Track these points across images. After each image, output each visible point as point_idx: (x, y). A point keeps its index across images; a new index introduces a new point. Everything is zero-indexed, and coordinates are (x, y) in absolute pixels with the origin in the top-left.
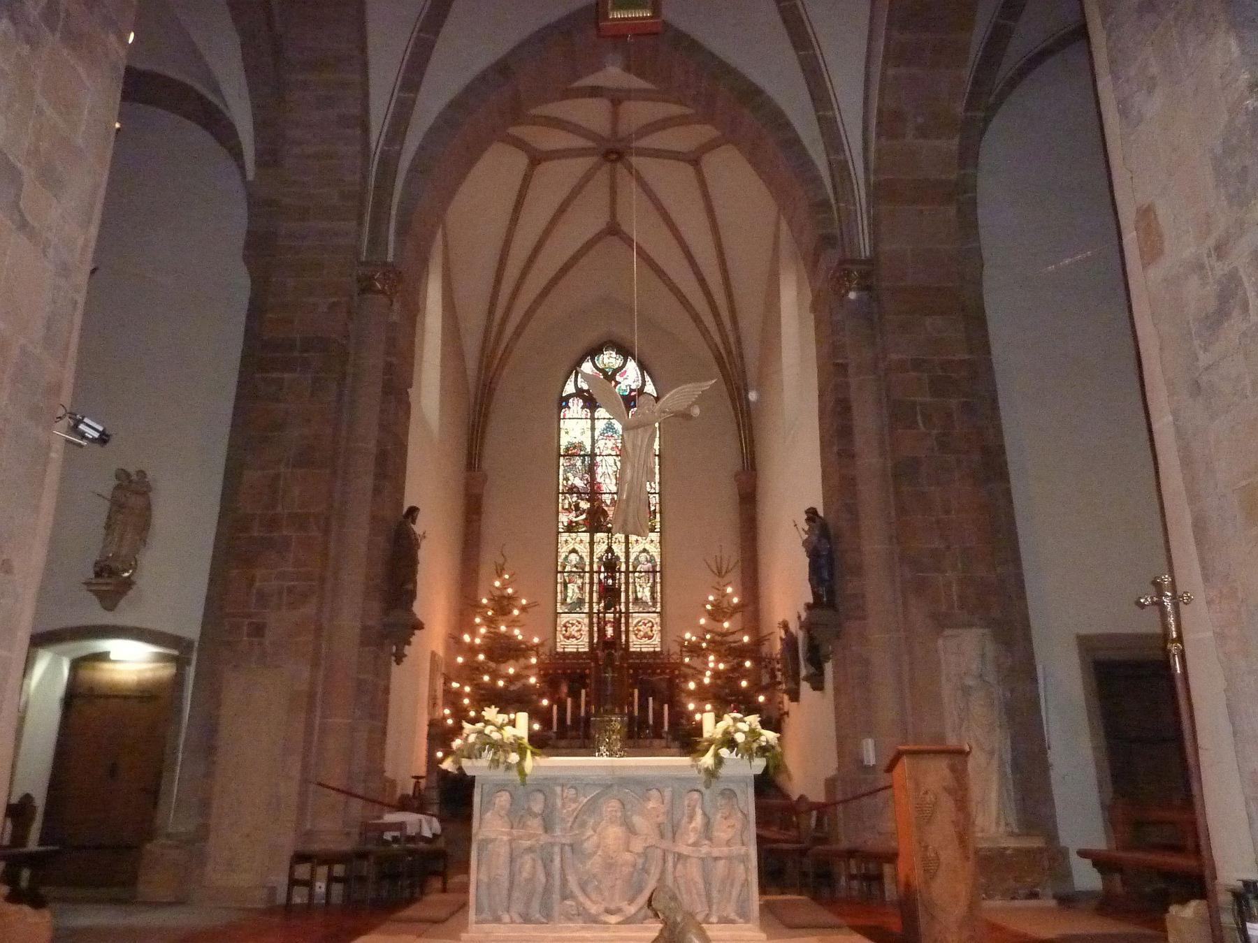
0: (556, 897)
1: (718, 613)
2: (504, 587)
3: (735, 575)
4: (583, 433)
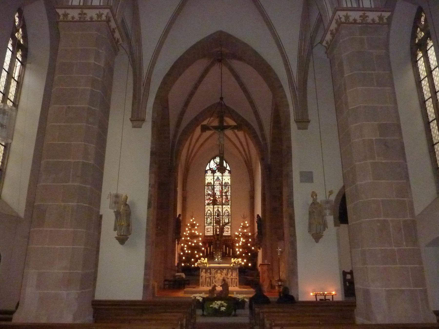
1: (244, 227)
2: (193, 221)
3: (248, 218)
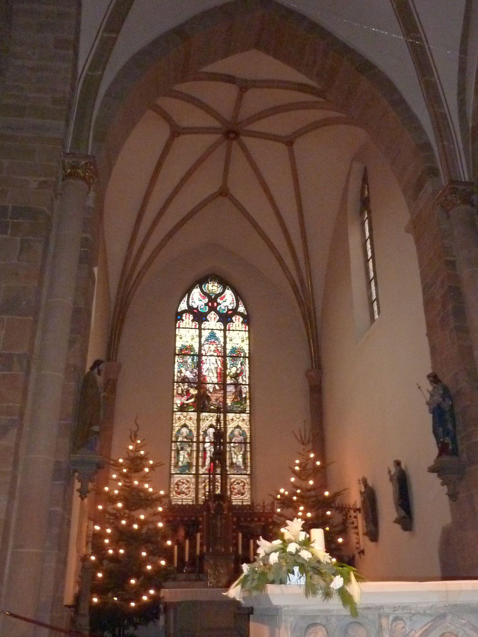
1: (302, 475)
2: (137, 449)
4: (193, 339)
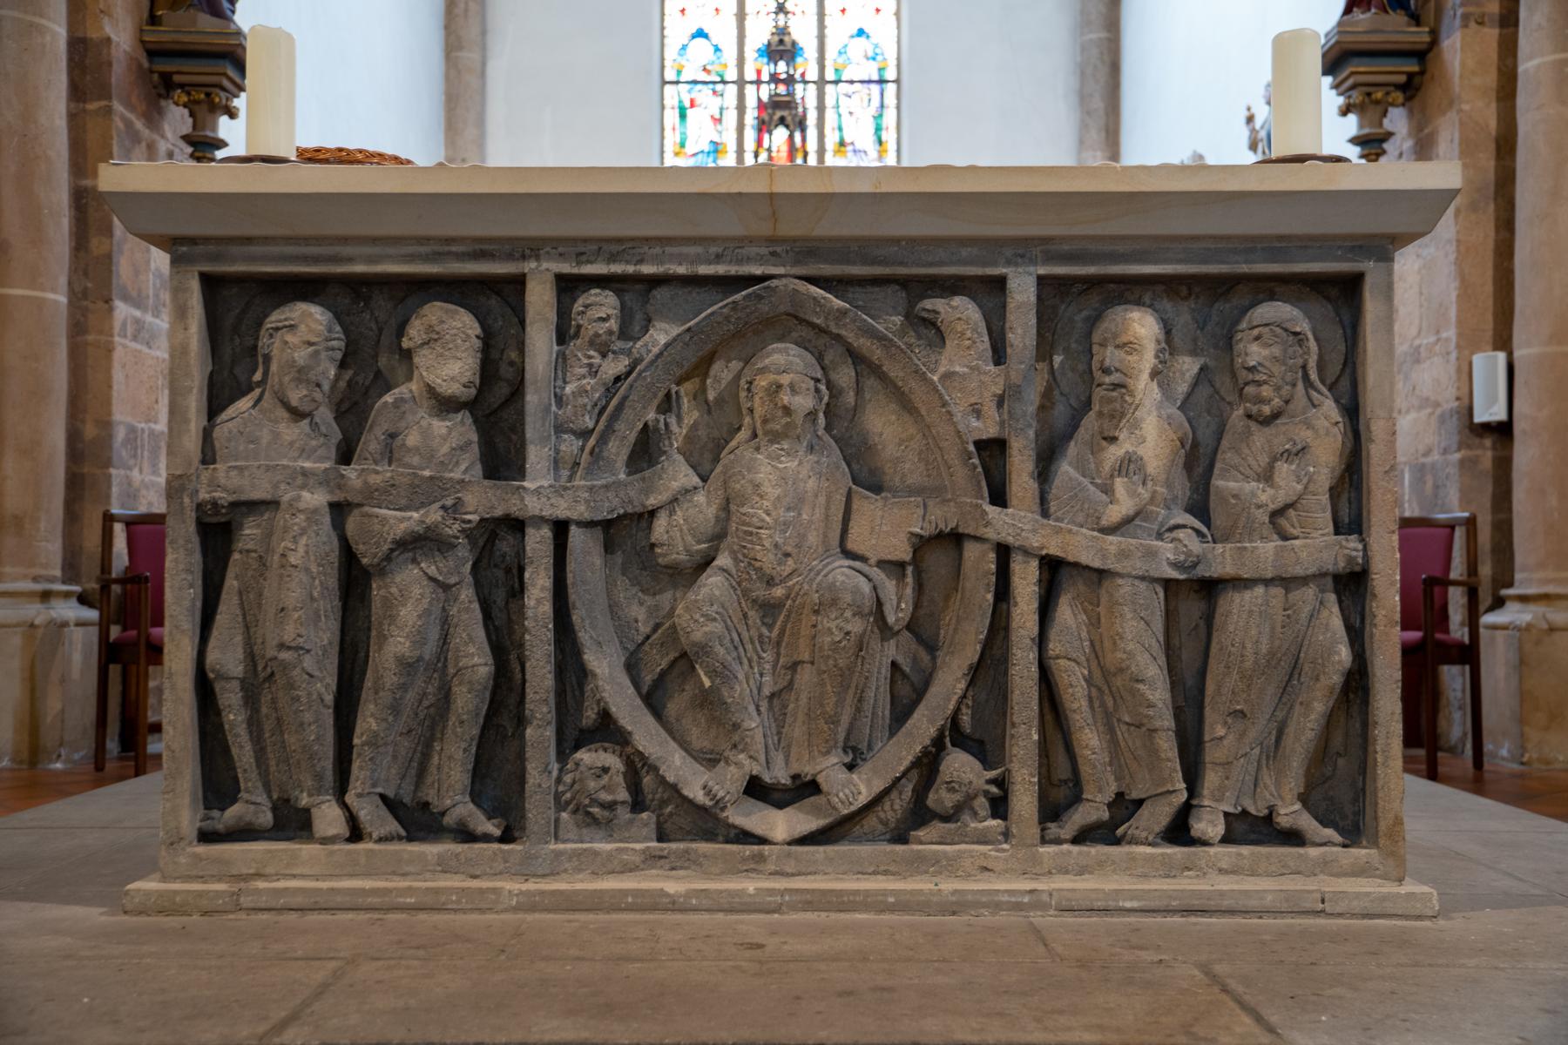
0: (540, 734)
